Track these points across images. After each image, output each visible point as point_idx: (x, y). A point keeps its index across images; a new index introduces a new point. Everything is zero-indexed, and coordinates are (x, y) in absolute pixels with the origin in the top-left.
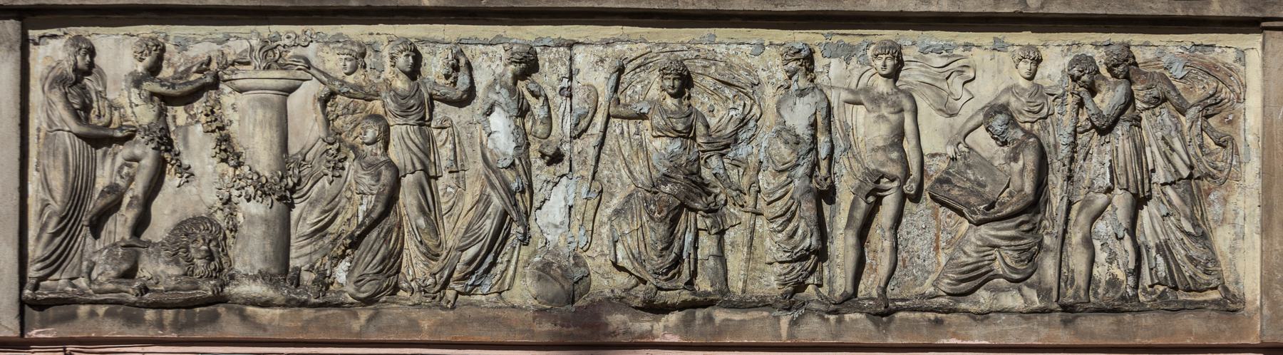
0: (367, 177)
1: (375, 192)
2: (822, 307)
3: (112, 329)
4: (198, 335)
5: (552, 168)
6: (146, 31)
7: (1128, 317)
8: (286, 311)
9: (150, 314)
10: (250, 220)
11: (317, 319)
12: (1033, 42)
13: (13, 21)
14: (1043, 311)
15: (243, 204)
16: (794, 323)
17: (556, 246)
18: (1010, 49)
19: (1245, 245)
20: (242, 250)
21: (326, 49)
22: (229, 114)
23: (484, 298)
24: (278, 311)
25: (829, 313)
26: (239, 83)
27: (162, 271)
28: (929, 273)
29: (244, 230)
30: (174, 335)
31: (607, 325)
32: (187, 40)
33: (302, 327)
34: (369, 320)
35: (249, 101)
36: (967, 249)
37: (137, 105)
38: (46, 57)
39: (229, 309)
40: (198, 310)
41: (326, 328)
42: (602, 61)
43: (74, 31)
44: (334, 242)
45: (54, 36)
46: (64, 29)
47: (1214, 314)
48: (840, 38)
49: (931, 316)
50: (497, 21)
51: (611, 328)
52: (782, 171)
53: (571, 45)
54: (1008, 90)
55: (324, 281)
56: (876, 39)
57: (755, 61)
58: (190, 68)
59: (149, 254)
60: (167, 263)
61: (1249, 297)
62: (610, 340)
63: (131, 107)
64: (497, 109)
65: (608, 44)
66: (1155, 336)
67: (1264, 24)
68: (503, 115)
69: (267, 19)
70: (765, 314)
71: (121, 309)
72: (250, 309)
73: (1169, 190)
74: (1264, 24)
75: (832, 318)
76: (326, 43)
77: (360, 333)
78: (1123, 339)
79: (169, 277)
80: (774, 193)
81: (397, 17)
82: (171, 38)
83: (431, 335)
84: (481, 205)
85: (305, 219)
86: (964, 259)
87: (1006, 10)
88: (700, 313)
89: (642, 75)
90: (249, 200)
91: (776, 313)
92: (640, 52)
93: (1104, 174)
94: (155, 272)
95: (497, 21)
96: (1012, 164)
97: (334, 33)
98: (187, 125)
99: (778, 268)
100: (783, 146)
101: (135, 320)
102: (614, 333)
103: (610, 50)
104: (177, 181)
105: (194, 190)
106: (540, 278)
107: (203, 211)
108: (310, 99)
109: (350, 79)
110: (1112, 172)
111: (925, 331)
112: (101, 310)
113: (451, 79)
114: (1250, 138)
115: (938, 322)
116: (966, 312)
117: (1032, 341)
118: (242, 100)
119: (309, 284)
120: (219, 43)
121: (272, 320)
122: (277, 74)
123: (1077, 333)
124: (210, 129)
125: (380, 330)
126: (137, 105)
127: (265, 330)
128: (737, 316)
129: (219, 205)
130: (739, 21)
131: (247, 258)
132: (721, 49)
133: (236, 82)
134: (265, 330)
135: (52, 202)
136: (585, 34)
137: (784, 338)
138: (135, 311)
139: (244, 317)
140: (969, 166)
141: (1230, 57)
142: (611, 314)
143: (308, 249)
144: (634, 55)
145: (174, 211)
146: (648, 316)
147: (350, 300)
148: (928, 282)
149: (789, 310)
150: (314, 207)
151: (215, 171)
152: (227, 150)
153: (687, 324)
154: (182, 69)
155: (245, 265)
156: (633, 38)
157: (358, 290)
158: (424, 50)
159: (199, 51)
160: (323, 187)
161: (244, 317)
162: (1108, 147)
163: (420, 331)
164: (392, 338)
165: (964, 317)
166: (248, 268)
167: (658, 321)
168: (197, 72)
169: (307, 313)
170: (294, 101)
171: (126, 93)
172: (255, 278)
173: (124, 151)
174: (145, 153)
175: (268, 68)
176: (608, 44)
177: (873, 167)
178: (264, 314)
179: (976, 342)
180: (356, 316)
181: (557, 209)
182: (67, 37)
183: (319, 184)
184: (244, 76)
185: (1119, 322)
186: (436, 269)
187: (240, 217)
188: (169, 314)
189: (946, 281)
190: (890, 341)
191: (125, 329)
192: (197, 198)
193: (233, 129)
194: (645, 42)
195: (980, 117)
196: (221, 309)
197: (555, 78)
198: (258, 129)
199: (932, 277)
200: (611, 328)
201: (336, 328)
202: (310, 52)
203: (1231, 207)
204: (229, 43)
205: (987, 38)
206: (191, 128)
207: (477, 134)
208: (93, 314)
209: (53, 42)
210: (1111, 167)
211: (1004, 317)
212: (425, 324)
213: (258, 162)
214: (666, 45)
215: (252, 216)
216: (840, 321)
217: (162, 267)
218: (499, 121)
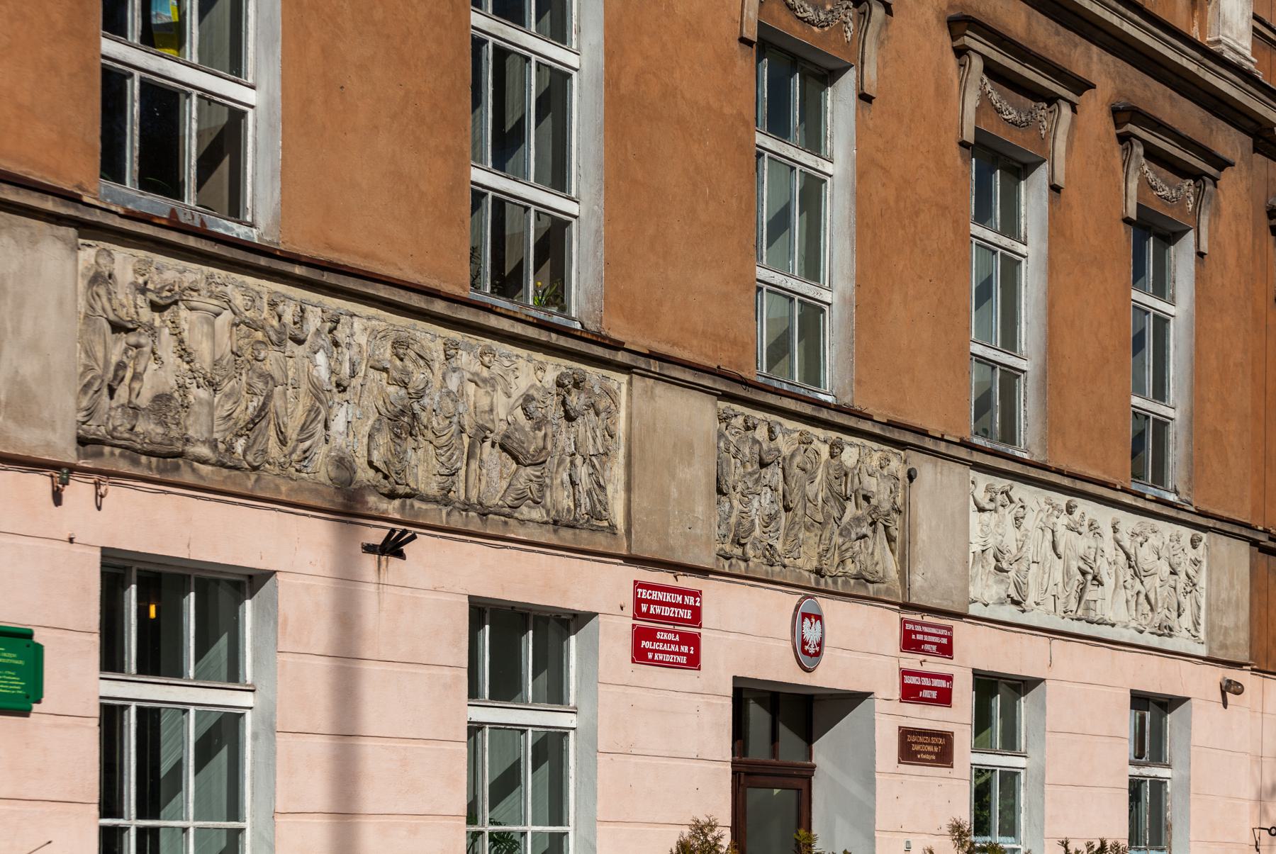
0: (261, 384)
1: (264, 394)
2: (461, 507)
3: (124, 467)
4: (171, 479)
5: (341, 395)
6: (142, 254)
7: (577, 531)
8: (214, 468)
9: (144, 459)
10: (200, 402)
11: (229, 477)
12: (543, 360)
13: (73, 229)
14: (546, 523)
15: (193, 388)
16: (448, 514)
17: (340, 447)
18: (534, 362)
19: (617, 496)
20: (195, 422)
21: (237, 290)
22: (185, 326)
23: (306, 475)
24: (210, 468)
25: (463, 510)
26: (194, 304)
27: (153, 430)
28: (498, 492)
29: (196, 408)
30: (158, 476)
31: (367, 502)
32: (163, 266)
33: (223, 481)
34: (257, 481)
35: (198, 318)
36: (520, 480)
37: (142, 307)
38: (85, 260)
39: (185, 462)
40: (169, 460)
41: (234, 484)
42: (366, 329)
43: (103, 245)
44: (236, 424)
45: (89, 246)
46: (96, 242)
47: (609, 535)
48: (468, 339)
49: (503, 518)
50: (129, 242)
51: (370, 505)
52: (447, 418)
53: (353, 315)
54: (533, 386)
55: (230, 449)
56: (482, 343)
57: (432, 345)
58: (165, 286)
59: (143, 416)
60: (157, 424)
61: (618, 527)
62: (369, 513)
63: (136, 308)
64: (321, 350)
65: (369, 319)
66: (588, 544)
67: (634, 370)
68: (324, 355)
69: (123, 240)
70: (435, 506)
71: (128, 452)
72: (196, 464)
73: (593, 458)
74: (634, 370)
75: (464, 513)
76: (237, 286)
77: (252, 490)
78: (576, 544)
79: (158, 434)
80: (443, 431)
81: (276, 278)
82: (155, 263)
83: (287, 496)
84: (313, 413)
85: (223, 406)
86: (519, 486)
87: (543, 339)
88: (408, 501)
89: (384, 342)
90: (198, 387)
91: (440, 507)
92: (384, 328)
93: (570, 444)
94: (147, 429)
95: (178, 254)
96: (537, 432)
97: (240, 280)
98: (161, 327)
99: (439, 478)
100: (450, 402)
101: (136, 463)
102: (370, 509)
103: (370, 323)
104: (156, 367)
105: (163, 374)
106: (338, 467)
107: (168, 391)
108: (227, 323)
109: (247, 314)
110: (575, 444)
111: (501, 528)
112: (117, 451)
113: (298, 326)
114: (621, 435)
115: (506, 523)
116: (517, 519)
117: (543, 540)
118: (195, 315)
119: (223, 451)
120: (180, 273)
121: (207, 474)
122: (216, 302)
123: (560, 538)
124: (174, 333)
125: (261, 489)
126: (142, 307)
127: (205, 480)
128: (424, 506)
129: (176, 387)
130: (152, 245)
131: (198, 427)
132: (418, 334)
133: (192, 303)
134: (205, 480)
135: (97, 368)
136: (360, 310)
137: (444, 524)
138: (135, 455)
139: (194, 470)
140: (516, 430)
141: (615, 386)
142: (369, 495)
143: (222, 427)
144: (381, 329)
145: (152, 387)
146: (386, 500)
147: (247, 466)
148: (498, 498)
149: (446, 505)
150: (229, 398)
151: (174, 363)
152: (185, 353)
153: (403, 506)
154: (158, 286)
155: (196, 432)
156: (381, 318)
157: (254, 460)
158: (309, 308)
159: (170, 276)
160: (234, 386)
161: (194, 470)
162: (573, 430)
163: (281, 493)
164: (268, 495)
165: (516, 521)
166: (199, 435)
167: (390, 503)
168: (167, 291)
169: (225, 472)
170: (219, 320)
171: (131, 297)
172: (204, 442)
173: (132, 338)
174: (148, 343)
175: (210, 297)
176: (369, 319)
177: (481, 422)
178: (205, 469)
179: (522, 538)
180: (248, 477)
181: (341, 422)
182: (98, 248)
183: (231, 383)
184: (196, 300)
185: (575, 534)
186: (286, 452)
187: (191, 398)
188: (154, 460)
189: (510, 498)
190: (489, 532)
191: (131, 467)
192: (164, 380)
193: (185, 335)
194: (385, 321)
195: (521, 401)
196: (181, 461)
197: (344, 335)
198: (204, 338)
199: (500, 495)
200: (370, 505)
201: (240, 484)
202: (229, 289)
203: (613, 473)
204: (185, 274)
205: (524, 353)
206: (163, 329)
207: (306, 364)
208: (112, 454)
209: (89, 250)
210: (575, 441)
211: (531, 524)
212: (283, 489)
213: (204, 361)
214: (394, 326)
215: (201, 399)
216: (467, 516)
217: (152, 426)
218: (321, 358)
